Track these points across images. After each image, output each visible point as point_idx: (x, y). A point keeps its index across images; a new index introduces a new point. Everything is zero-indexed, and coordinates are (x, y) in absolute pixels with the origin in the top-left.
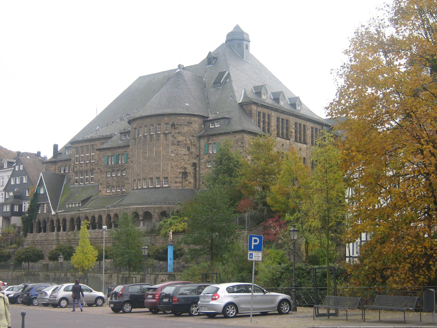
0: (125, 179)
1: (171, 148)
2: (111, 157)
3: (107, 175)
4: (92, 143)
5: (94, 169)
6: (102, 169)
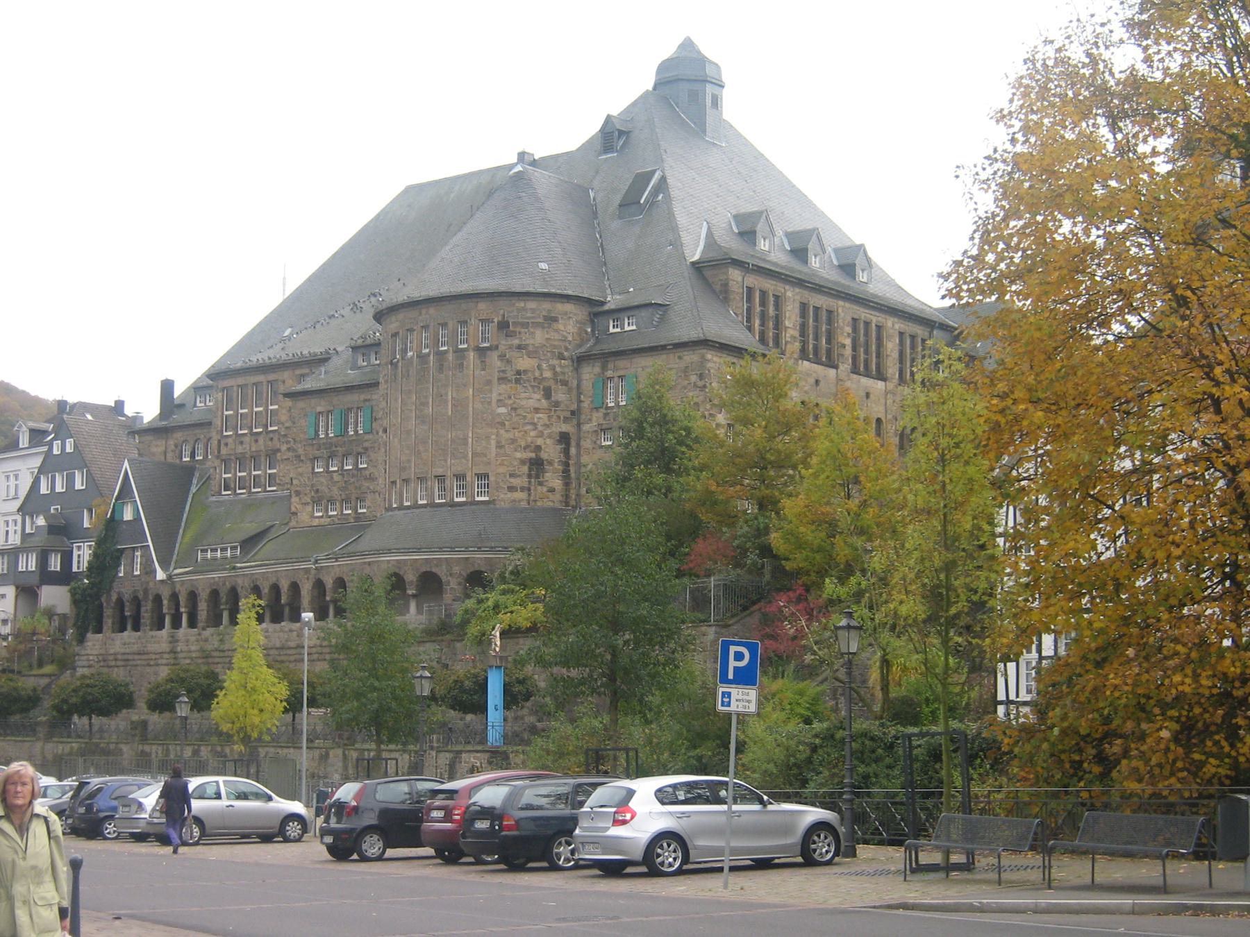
0: (366, 479)
1: (498, 390)
2: (325, 414)
3: (313, 469)
4: (272, 377)
5: (279, 450)
6: (301, 451)
